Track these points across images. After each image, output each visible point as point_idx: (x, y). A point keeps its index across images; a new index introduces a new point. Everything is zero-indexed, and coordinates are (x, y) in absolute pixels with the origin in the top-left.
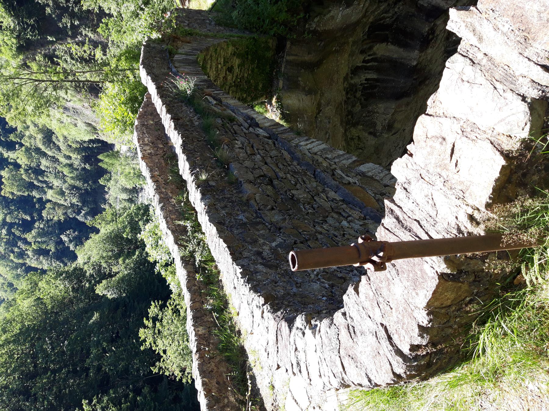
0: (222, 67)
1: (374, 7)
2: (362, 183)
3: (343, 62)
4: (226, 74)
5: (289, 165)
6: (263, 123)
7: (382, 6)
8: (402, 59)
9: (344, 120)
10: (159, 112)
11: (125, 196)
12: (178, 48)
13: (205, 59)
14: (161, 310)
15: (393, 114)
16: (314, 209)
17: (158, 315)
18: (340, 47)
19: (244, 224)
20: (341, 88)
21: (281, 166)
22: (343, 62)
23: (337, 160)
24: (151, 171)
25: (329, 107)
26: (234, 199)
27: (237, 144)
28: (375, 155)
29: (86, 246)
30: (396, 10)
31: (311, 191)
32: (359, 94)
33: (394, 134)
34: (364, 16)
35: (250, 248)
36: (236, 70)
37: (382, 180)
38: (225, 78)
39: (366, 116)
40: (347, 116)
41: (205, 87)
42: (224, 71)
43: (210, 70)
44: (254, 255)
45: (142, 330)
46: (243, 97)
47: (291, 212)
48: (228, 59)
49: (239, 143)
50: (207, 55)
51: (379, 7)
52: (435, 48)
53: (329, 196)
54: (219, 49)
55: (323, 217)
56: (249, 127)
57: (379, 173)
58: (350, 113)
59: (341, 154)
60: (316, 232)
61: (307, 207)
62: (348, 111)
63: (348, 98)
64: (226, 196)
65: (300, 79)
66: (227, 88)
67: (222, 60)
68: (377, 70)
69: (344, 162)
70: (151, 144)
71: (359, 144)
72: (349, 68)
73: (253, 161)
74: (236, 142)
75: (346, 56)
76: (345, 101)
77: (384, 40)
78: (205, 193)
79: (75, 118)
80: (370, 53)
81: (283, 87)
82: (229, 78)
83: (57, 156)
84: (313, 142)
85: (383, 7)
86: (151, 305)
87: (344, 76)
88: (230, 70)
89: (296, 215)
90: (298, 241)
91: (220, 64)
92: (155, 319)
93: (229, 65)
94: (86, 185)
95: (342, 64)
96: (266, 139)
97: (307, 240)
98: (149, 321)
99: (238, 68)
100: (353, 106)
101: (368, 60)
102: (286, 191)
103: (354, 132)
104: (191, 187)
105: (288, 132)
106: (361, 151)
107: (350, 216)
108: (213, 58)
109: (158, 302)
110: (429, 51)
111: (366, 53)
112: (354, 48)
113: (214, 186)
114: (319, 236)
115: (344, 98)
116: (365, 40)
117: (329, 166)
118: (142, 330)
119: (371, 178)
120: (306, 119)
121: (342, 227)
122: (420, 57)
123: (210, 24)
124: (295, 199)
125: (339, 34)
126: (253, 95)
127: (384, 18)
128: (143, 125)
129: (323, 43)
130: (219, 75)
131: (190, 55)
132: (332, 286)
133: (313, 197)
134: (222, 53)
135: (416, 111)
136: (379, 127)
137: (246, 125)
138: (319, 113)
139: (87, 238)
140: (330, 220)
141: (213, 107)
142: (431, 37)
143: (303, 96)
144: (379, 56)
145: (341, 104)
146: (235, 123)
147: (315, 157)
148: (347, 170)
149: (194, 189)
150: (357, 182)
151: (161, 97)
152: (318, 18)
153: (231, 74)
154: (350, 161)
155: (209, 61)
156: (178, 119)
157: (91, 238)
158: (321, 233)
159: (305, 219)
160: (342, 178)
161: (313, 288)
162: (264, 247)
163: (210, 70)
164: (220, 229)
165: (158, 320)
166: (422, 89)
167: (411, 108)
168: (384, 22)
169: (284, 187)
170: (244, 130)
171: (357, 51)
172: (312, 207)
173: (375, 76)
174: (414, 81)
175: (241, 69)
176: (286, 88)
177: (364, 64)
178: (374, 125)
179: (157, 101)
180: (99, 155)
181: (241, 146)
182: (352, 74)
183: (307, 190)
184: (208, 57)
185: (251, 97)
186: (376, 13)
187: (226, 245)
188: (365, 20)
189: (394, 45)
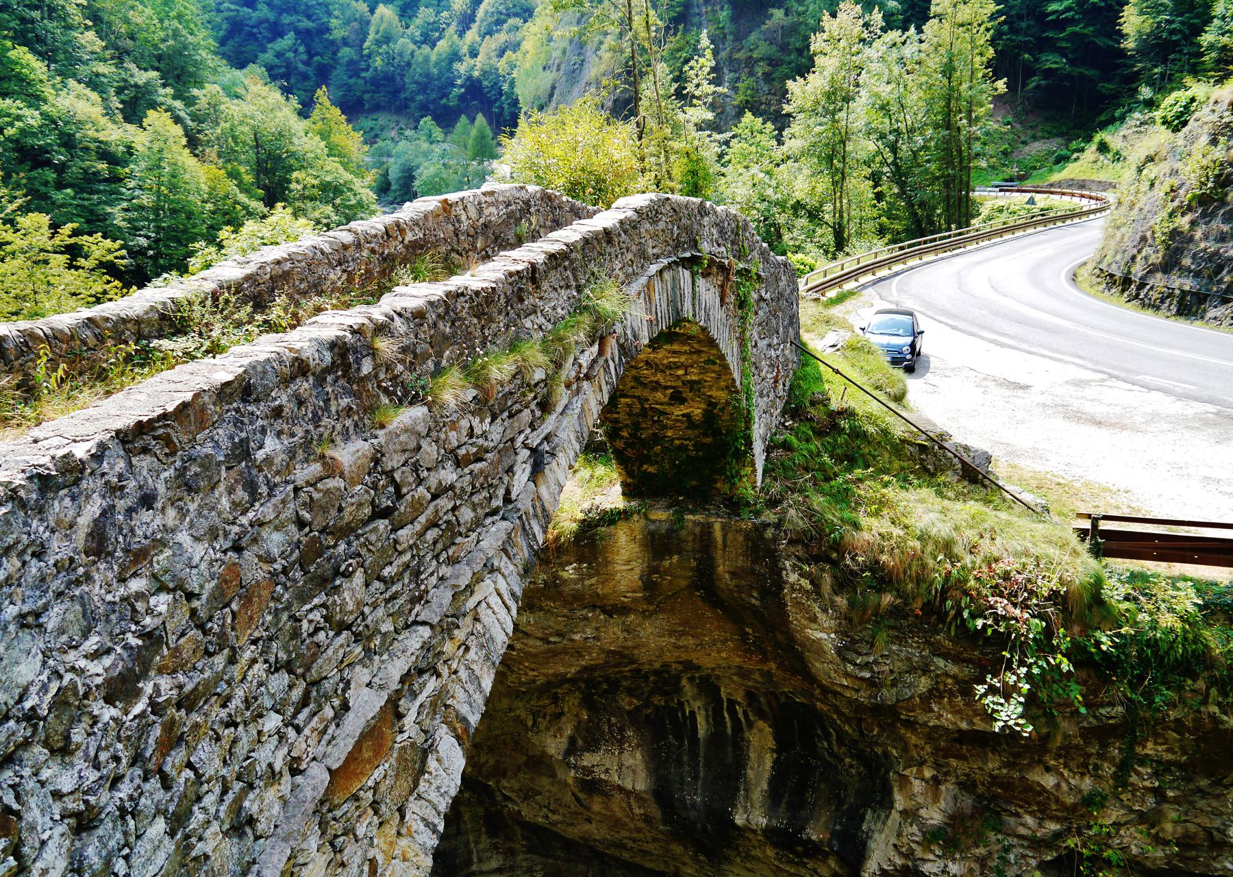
0: (678, 377)
1: (846, 711)
2: (403, 748)
4: (666, 388)
5: (437, 557)
7: (850, 726)
8: (746, 790)
9: (596, 674)
13: (690, 337)
14: (101, 264)
15: (620, 789)
16: (311, 635)
17: (86, 257)
20: (668, 657)
22: (724, 655)
23: (463, 674)
25: (621, 635)
26: (325, 421)
27: (482, 421)
28: (524, 758)
30: (848, 760)
31: (364, 620)
32: (658, 700)
33: (578, 800)
34: (825, 690)
35: (166, 474)
36: (678, 411)
37: (419, 797)
38: (656, 386)
39: (610, 726)
40: (607, 679)
41: (622, 341)
45: (44, 219)
46: (621, 429)
49: (486, 426)
50: (699, 342)
51: (848, 720)
52: (776, 863)
53: (358, 668)
54: (717, 368)
57: (438, 788)
58: (614, 686)
59: (483, 685)
60: (233, 649)
62: (618, 681)
63: (646, 677)
64: (333, 403)
65: (675, 558)
67: (695, 378)
68: (717, 737)
71: (544, 717)
72: (713, 669)
73: (440, 464)
74: (488, 420)
76: (638, 671)
77: (782, 745)
78: (336, 350)
79: (562, 67)
81: (654, 522)
83: (475, 27)
85: (850, 731)
87: (695, 661)
88: (678, 398)
89: (286, 588)
90: (196, 604)
91: (686, 374)
92: (74, 252)
93: (688, 394)
94: (414, 87)
95: (719, 652)
98: (70, 237)
99: (683, 415)
100: (630, 692)
102: (359, 555)
104: (356, 316)
105: (531, 546)
106: (530, 723)
107: (299, 730)
108: (695, 357)
110: (770, 852)
111: (749, 705)
112: (757, 676)
113: (359, 369)
114: (220, 660)
116: (778, 699)
117: (444, 657)
118: (44, 219)
119: (422, 770)
120: (587, 583)
121: (261, 716)
122: (754, 832)
123: (769, 345)
124: (338, 582)
125: (780, 637)
127: (827, 736)
128: (527, 203)
130: (662, 371)
131: (693, 305)
134: (709, 377)
135: (635, 841)
136: (588, 760)
137: (534, 441)
138: (604, 611)
139: (287, 91)
140: (280, 681)
141: (571, 360)
142: (800, 849)
143: (638, 571)
144: (747, 734)
146: (538, 413)
147: (469, 620)
148: (439, 702)
150: (406, 735)
152: (809, 587)
155: (687, 348)
156: (533, 280)
157: (288, 99)
158: (232, 661)
159: (277, 613)
160: (414, 695)
164: (228, 391)
166: (685, 847)
167: (639, 830)
168: (818, 736)
170: (522, 437)
171: (751, 683)
172: (317, 630)
173: (702, 732)
174: (699, 826)
176: (652, 527)
178: (592, 745)
181: (478, 431)
183: (367, 610)
184: (696, 346)
185: (625, 449)
186: (835, 717)
189: (773, 768)
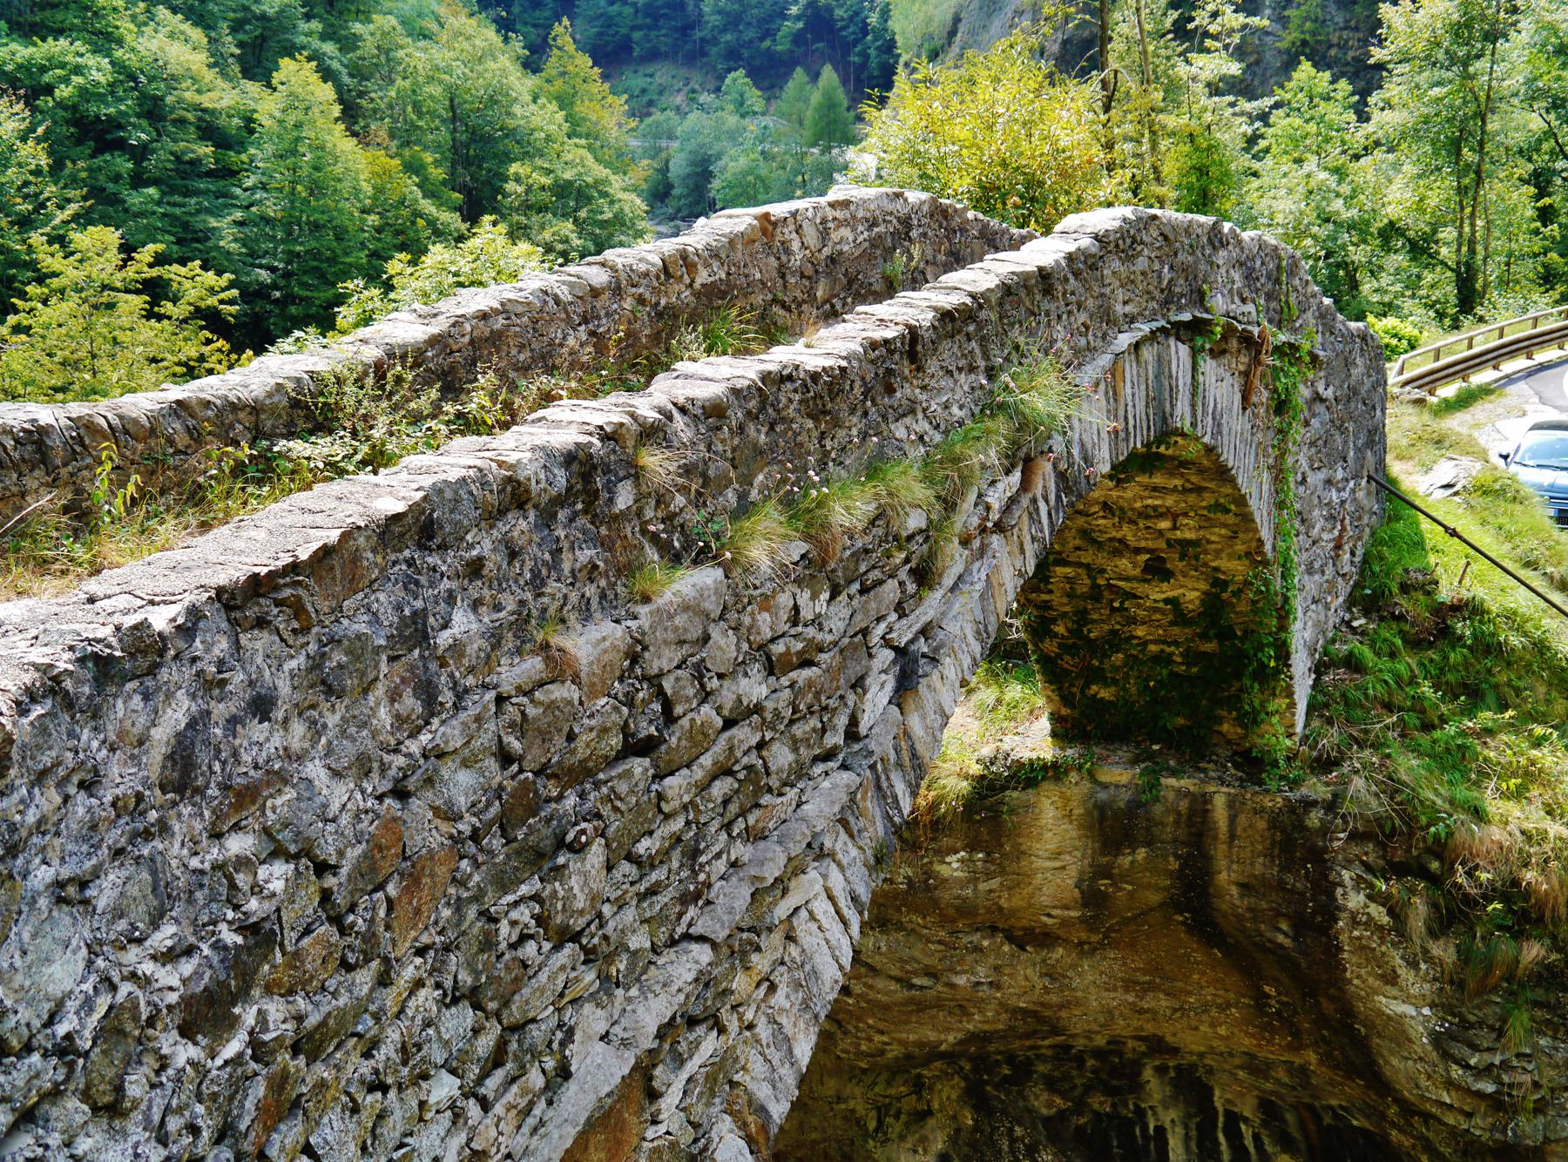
0: (1161, 533)
3: (1222, 1031)
4: (1138, 551)
5: (728, 827)
6: (920, 707)
10: (943, 278)
11: (679, 167)
12: (1217, 353)
13: (1184, 464)
14: (199, 313)
16: (513, 946)
17: (175, 300)
18: (1279, 1013)
19: (426, 637)
20: (1121, 1027)
21: (720, 788)
22: (1222, 1031)
23: (764, 1031)
24: (714, 253)
26: (552, 586)
27: (814, 597)
29: (473, 22)
31: (601, 926)
34: (1407, 1109)
35: (293, 664)
36: (1158, 593)
38: (1120, 548)
39: (1013, 1141)
40: (1011, 1059)
42: (1150, 544)
43: (1146, 488)
44: (251, 684)
46: (1054, 621)
47: (496, 842)
48: (1197, 558)
53: (588, 1008)
54: (1231, 519)
55: (475, 990)
56: (896, 649)
58: (1022, 1071)
59: (797, 1052)
60: (386, 960)
61: (524, 914)
63: (1080, 1060)
64: (566, 556)
65: (1142, 853)
66: (1086, 558)
69: (758, 1066)
70: (826, 251)
71: (897, 1116)
72: (1202, 1055)
73: (740, 666)
74: (825, 596)
75: (1247, 1041)
76: (1067, 1048)
78: (575, 467)
80: (1266, 1140)
82: (1124, 564)
84: (845, 923)
86: (219, 273)
87: (1169, 1039)
88: (1157, 570)
89: (477, 865)
90: (330, 881)
91: (1175, 528)
92: (156, 291)
93: (1175, 564)
95: (1213, 1025)
96: (842, 721)
97: (337, 920)
98: (151, 266)
99: (1167, 601)
100: (1051, 1084)
101: (1240, 1136)
102: (598, 816)
103: (947, 1093)
104: (608, 411)
106: (872, 1125)
107: (485, 1105)
108: (1192, 498)
109: (231, 302)
112: (1281, 1074)
113: (611, 501)
115: (1080, 1043)
116: (1318, 1118)
117: (733, 999)
118: (111, 237)
120: (983, 886)
121: (425, 1077)
126: (1068, 662)
128: (906, 222)
129: (1287, 942)
131: (1193, 406)
132: (65, 1050)
133: (575, 937)
134: (1216, 535)
137: (903, 636)
138: (1010, 939)
140: (460, 1019)
143: (1073, 871)
145: (1056, 1031)
146: (911, 587)
149: (599, 419)
150: (662, 1129)
151: (1006, 290)
153: (1137, 572)
154: (763, 1092)
155: (1178, 482)
156: (912, 356)
157: (506, 40)
158: (384, 980)
159: (459, 906)
160: (680, 1061)
161: (48, 961)
162: (298, 728)
163: (1146, 488)
164: (397, 529)
165: (154, 303)
169: (616, 809)
171: (1269, 1086)
172: (524, 938)
175: (1163, 612)
177: (1221, 1119)
179: (988, 272)
180: (836, 69)
181: (806, 614)
182: (1178, 1068)
183: (607, 910)
184: (1194, 479)
185: (1059, 656)
187: (304, 556)
188: (1393, 1111)
